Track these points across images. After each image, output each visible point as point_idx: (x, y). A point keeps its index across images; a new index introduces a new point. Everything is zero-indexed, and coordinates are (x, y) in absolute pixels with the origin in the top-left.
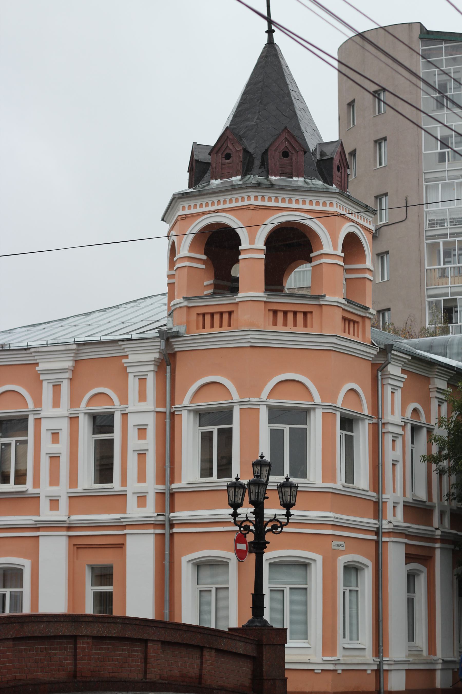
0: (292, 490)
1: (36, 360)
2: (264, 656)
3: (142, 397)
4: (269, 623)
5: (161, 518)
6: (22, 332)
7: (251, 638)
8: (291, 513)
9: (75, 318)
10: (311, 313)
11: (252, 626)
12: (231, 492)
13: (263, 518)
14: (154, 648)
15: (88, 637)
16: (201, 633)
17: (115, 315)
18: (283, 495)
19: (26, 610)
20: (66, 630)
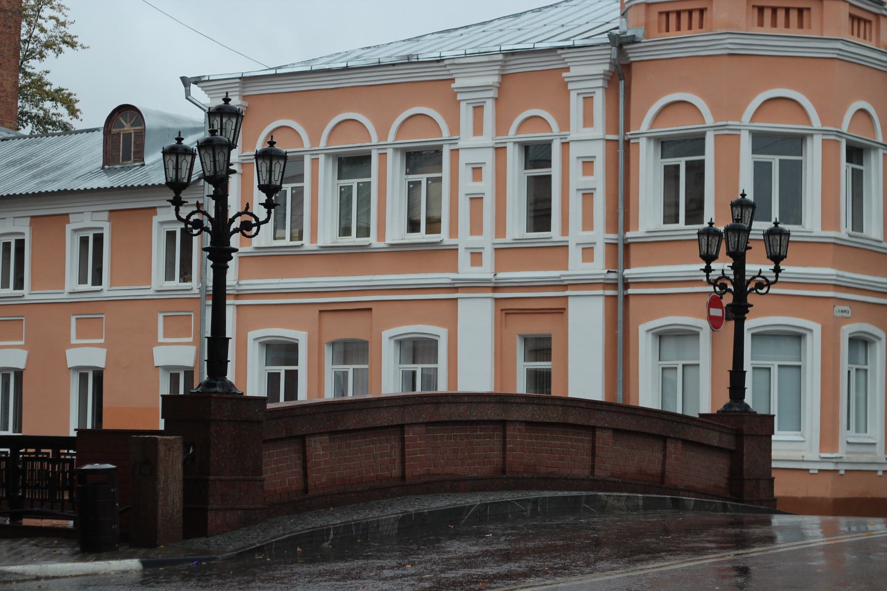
0: (783, 238)
1: (452, 74)
2: (745, 450)
3: (588, 121)
4: (751, 407)
5: (612, 276)
6: (433, 39)
7: (727, 426)
8: (712, 268)
9: (501, 21)
10: (809, 9)
11: (729, 412)
12: (703, 240)
13: (744, 275)
14: (604, 438)
15: (521, 422)
16: (664, 419)
17: (552, 16)
18: (771, 244)
19: (442, 387)
20: (493, 412)
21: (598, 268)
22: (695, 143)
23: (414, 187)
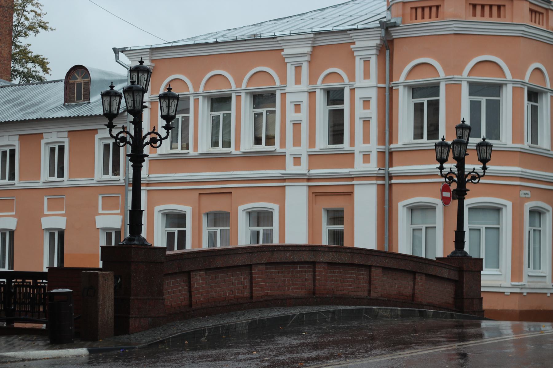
0: (488, 148)
1: (282, 46)
2: (464, 280)
3: (367, 75)
4: (468, 253)
5: (382, 172)
6: (270, 25)
7: (453, 265)
8: (444, 167)
9: (312, 13)
10: (504, 6)
11: (455, 256)
12: (438, 150)
13: (464, 171)
14: (376, 273)
15: (325, 263)
16: (414, 261)
17: (344, 10)
18: (481, 152)
19: (276, 241)
20: (307, 257)
21: (373, 167)
22: (434, 89)
23: (258, 116)
